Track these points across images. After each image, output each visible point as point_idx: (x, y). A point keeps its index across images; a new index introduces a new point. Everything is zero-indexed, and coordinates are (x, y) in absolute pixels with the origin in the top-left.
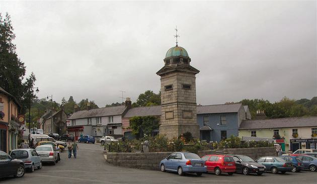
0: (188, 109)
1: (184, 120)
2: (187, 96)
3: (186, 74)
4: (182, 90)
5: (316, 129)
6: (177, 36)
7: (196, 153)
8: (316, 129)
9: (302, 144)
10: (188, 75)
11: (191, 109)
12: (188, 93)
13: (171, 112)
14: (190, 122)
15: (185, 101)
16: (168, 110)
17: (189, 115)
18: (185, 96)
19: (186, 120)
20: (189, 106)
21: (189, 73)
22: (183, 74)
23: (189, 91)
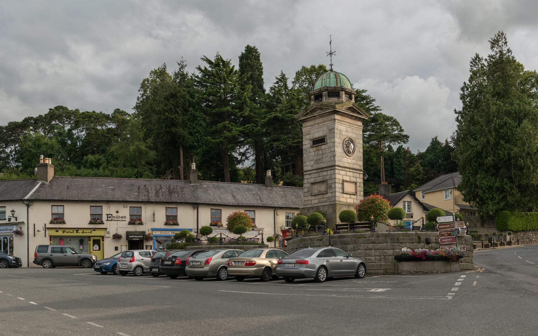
0: (320, 179)
1: (313, 198)
2: (320, 157)
3: (318, 121)
4: (311, 150)
5: (306, 171)
6: (331, 54)
7: (55, 173)
8: (306, 171)
9: (324, 93)
10: (321, 120)
11: (327, 177)
12: (321, 152)
13: (343, 184)
14: (324, 200)
15: (316, 166)
16: (347, 179)
17: (323, 188)
18: (315, 158)
19: (317, 197)
20: (321, 174)
21: (321, 116)
22: (311, 123)
23: (323, 147)
